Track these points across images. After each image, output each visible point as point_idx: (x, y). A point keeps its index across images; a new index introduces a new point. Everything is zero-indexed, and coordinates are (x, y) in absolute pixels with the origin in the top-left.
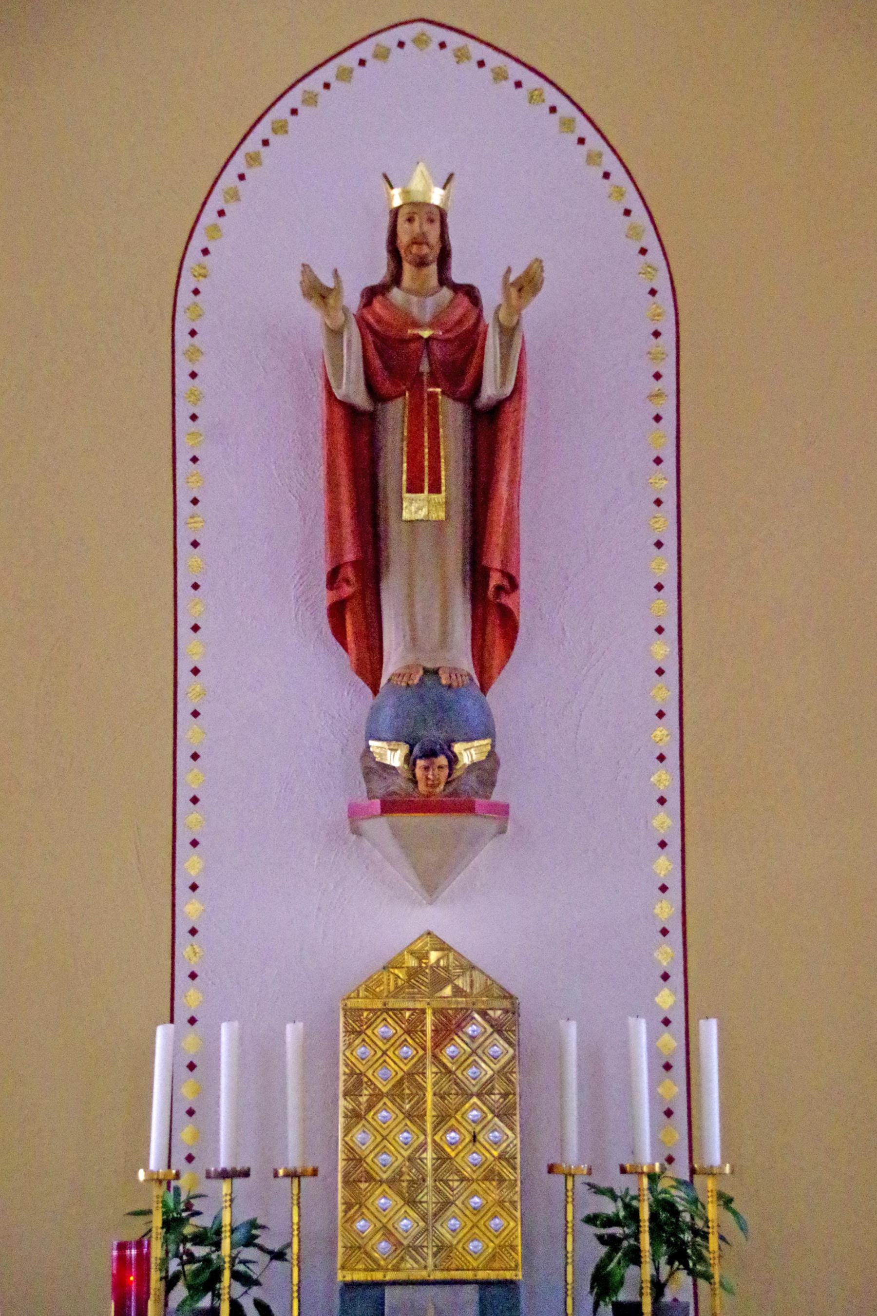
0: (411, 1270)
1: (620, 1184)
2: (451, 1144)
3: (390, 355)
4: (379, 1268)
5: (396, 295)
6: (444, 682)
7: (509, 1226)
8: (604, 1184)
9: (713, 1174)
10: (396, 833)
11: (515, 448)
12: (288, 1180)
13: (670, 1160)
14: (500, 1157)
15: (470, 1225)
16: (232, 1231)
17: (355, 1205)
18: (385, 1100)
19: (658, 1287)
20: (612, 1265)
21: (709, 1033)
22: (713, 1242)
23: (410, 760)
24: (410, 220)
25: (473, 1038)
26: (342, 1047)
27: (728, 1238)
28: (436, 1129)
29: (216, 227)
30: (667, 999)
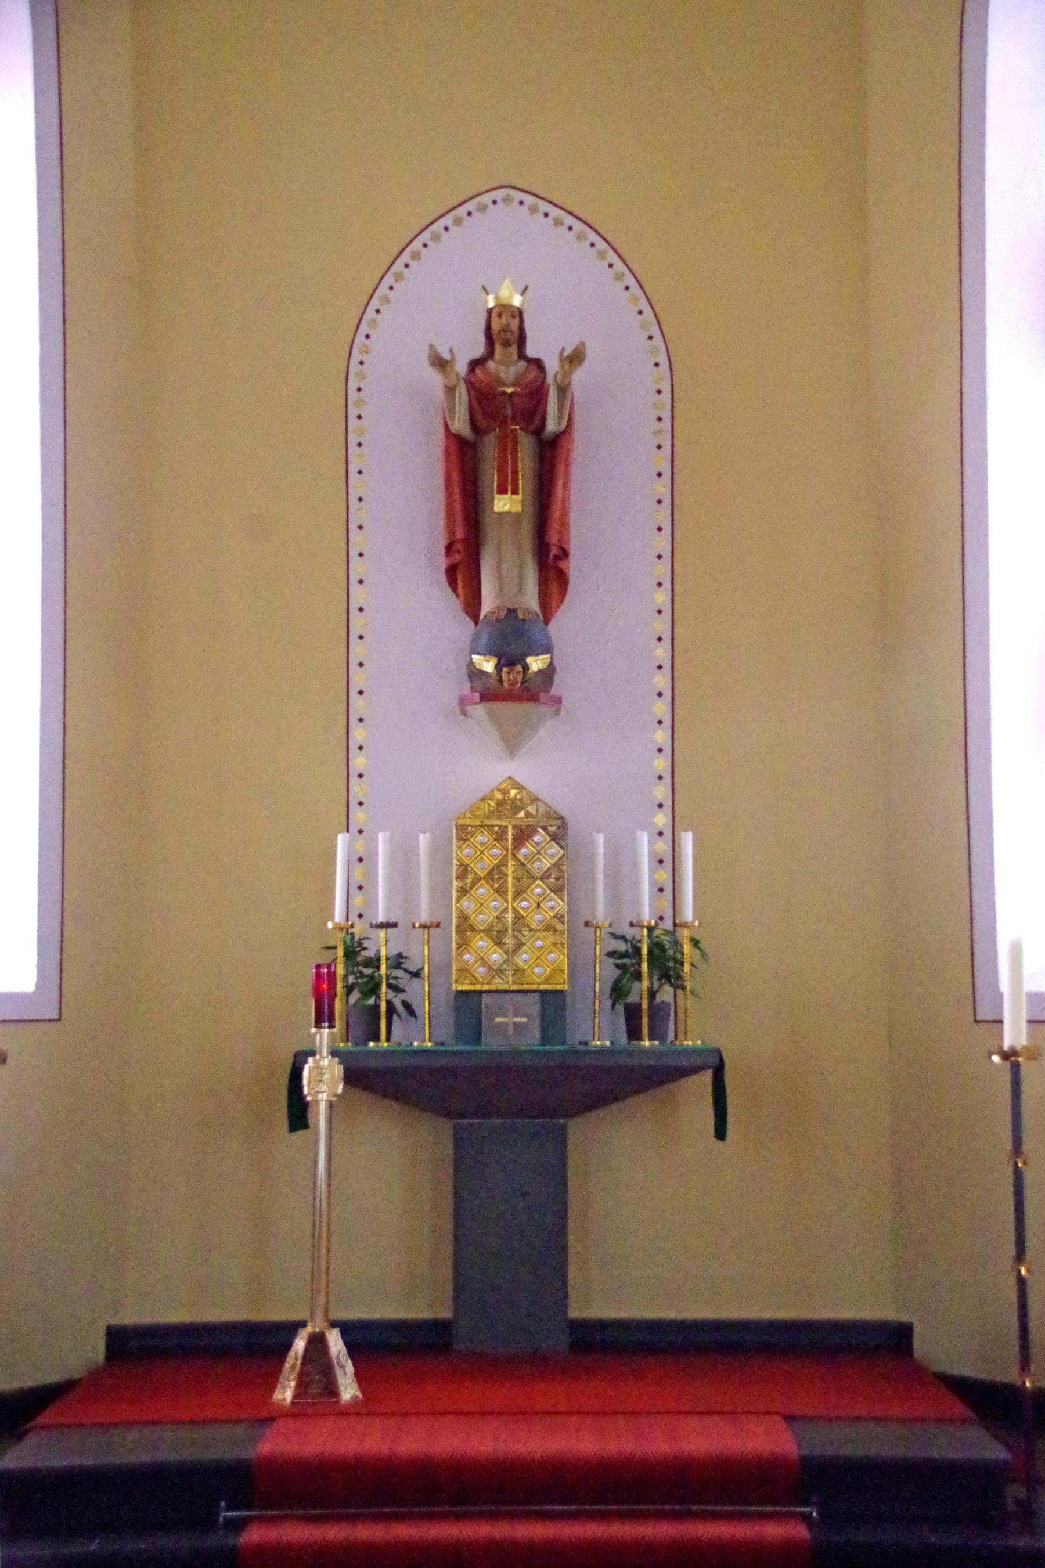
0: (498, 984)
1: (629, 932)
2: (523, 908)
3: (484, 400)
4: (479, 983)
5: (491, 365)
6: (520, 617)
7: (560, 958)
8: (619, 933)
9: (687, 927)
10: (490, 714)
11: (567, 466)
12: (421, 930)
13: (661, 918)
14: (554, 917)
15: (535, 957)
16: (387, 959)
17: (464, 944)
18: (482, 881)
19: (652, 994)
20: (625, 981)
21: (687, 840)
22: (687, 968)
23: (498, 667)
24: (500, 316)
25: (538, 844)
26: (455, 849)
27: (696, 965)
28: (514, 899)
29: (374, 321)
30: (662, 819)
